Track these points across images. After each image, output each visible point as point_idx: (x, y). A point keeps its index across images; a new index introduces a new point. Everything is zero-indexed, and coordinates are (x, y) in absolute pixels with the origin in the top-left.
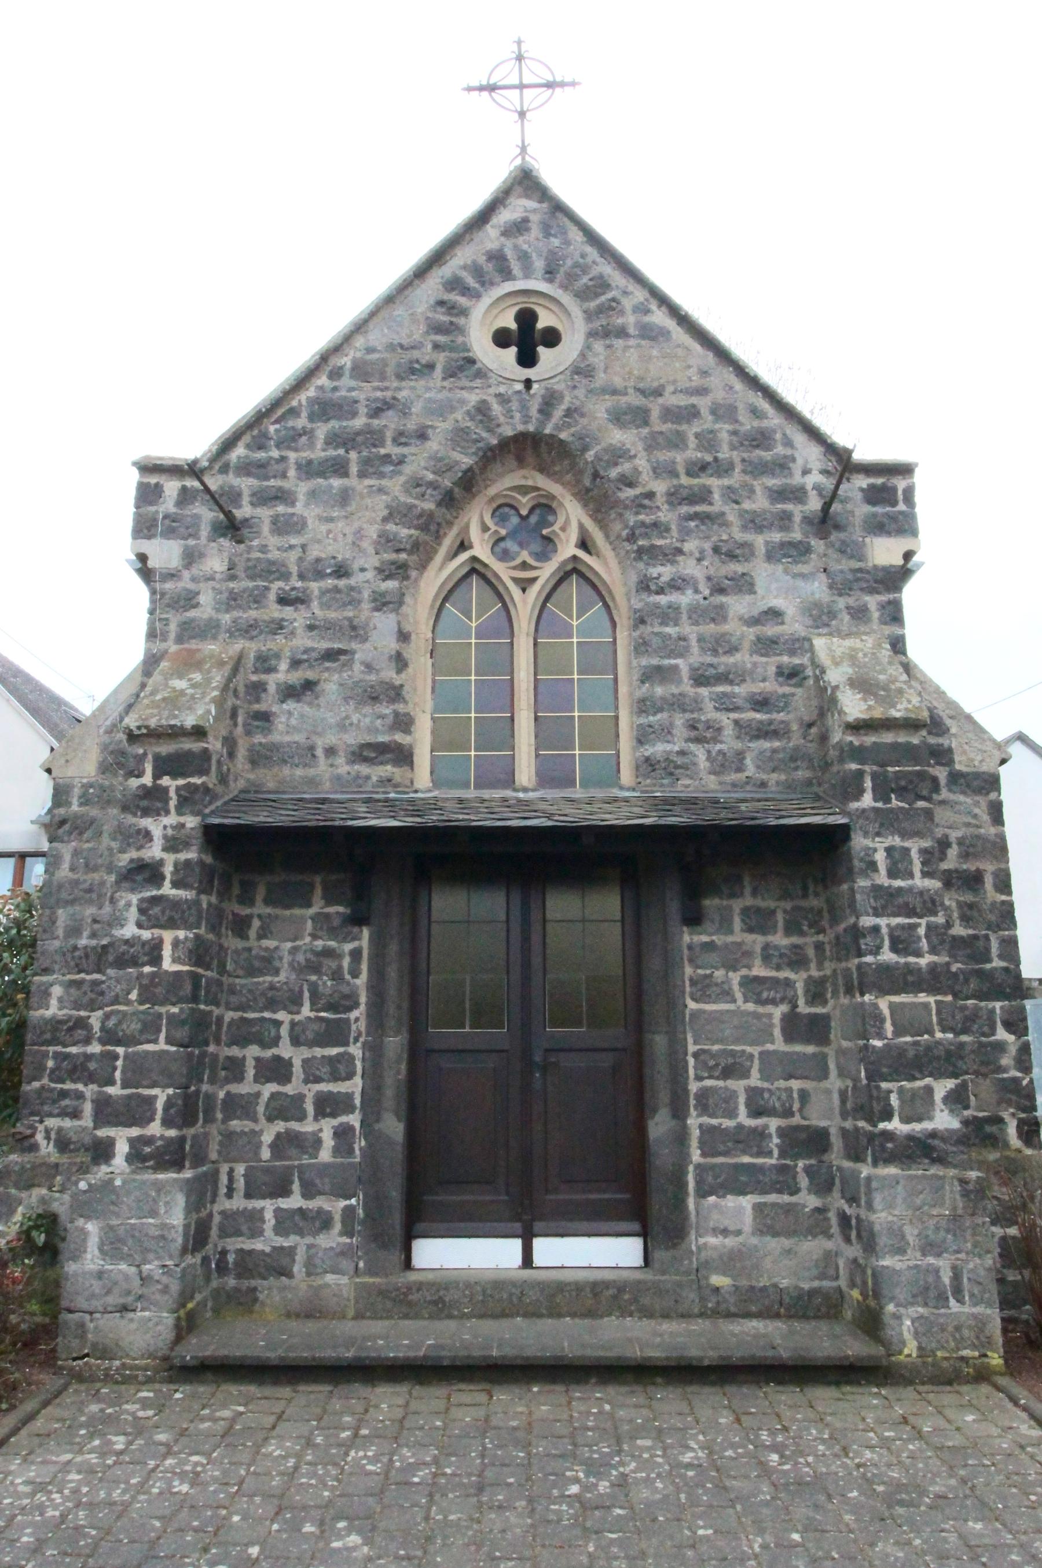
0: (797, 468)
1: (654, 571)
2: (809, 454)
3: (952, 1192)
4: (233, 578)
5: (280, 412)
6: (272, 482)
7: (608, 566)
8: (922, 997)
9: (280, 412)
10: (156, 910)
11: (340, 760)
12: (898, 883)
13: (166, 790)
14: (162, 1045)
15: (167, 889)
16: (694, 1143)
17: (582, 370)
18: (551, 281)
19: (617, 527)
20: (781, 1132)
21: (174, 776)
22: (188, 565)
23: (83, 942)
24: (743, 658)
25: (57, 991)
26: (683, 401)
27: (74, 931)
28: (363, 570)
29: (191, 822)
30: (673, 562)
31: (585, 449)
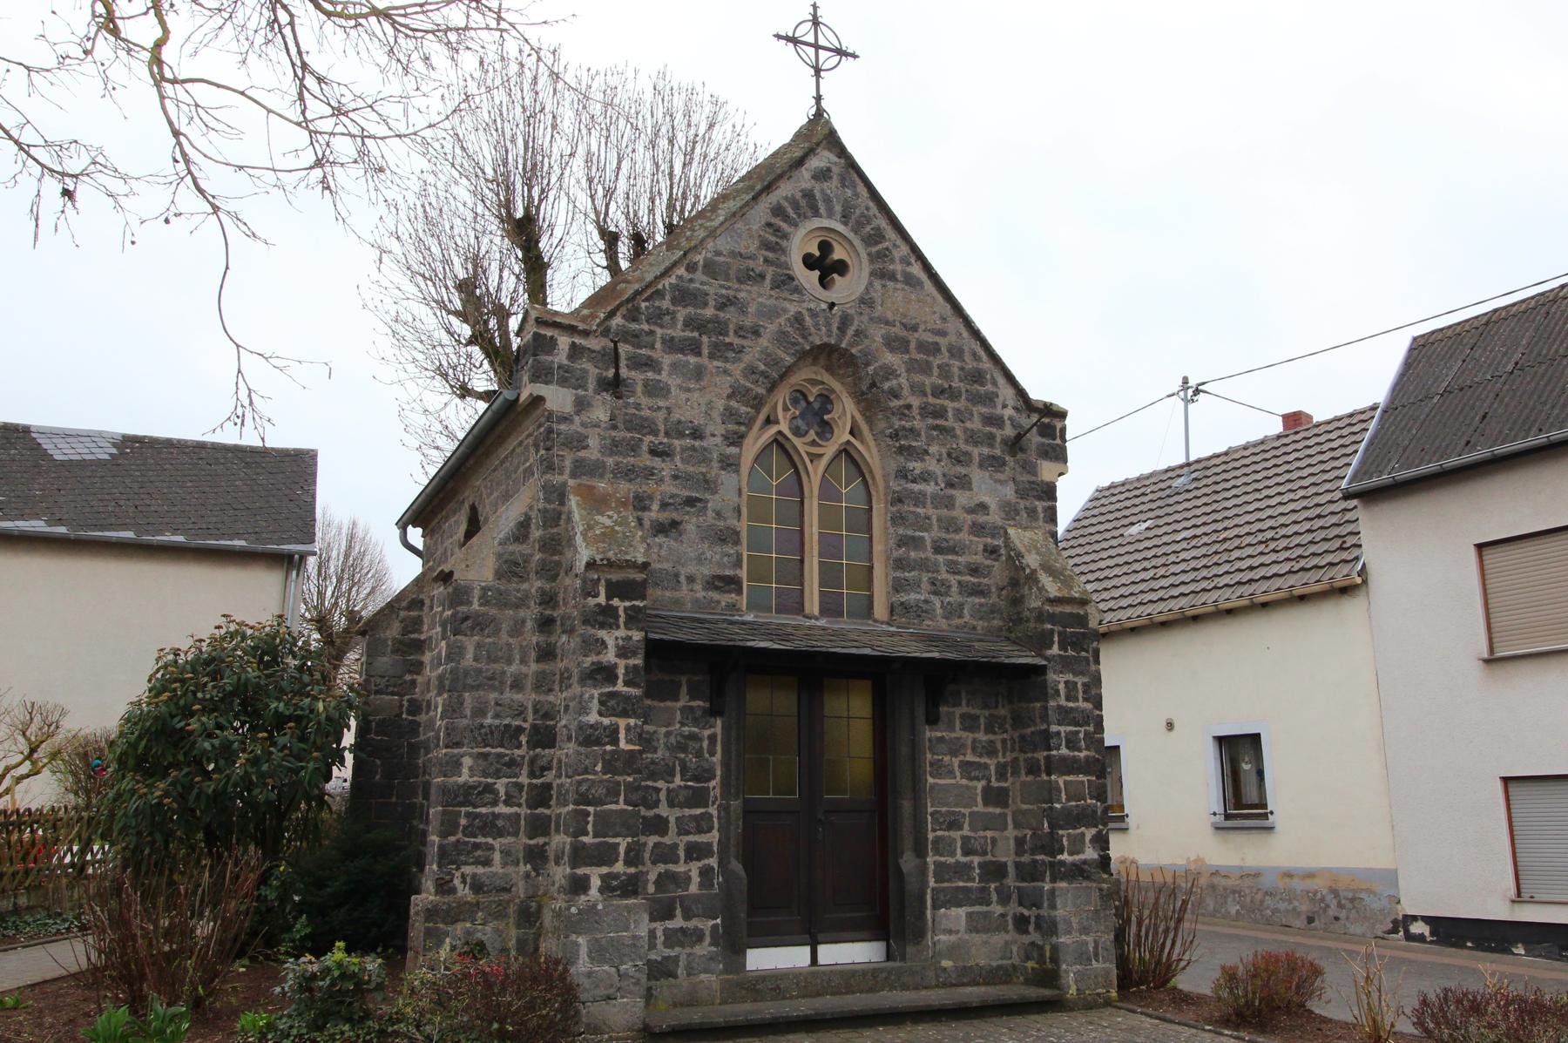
0: (999, 402)
1: (911, 465)
2: (1007, 393)
3: (1095, 895)
4: (615, 427)
5: (649, 292)
6: (643, 351)
7: (871, 453)
8: (1081, 778)
9: (649, 292)
10: (612, 703)
11: (698, 587)
12: (1071, 704)
13: (616, 608)
14: (622, 806)
15: (620, 687)
16: (931, 874)
17: (866, 301)
18: (845, 224)
19: (882, 425)
20: (981, 866)
21: (622, 599)
22: (578, 413)
23: (488, 721)
24: (964, 536)
25: (467, 762)
26: (930, 338)
27: (480, 712)
28: (713, 435)
29: (637, 636)
30: (923, 460)
31: (867, 364)
